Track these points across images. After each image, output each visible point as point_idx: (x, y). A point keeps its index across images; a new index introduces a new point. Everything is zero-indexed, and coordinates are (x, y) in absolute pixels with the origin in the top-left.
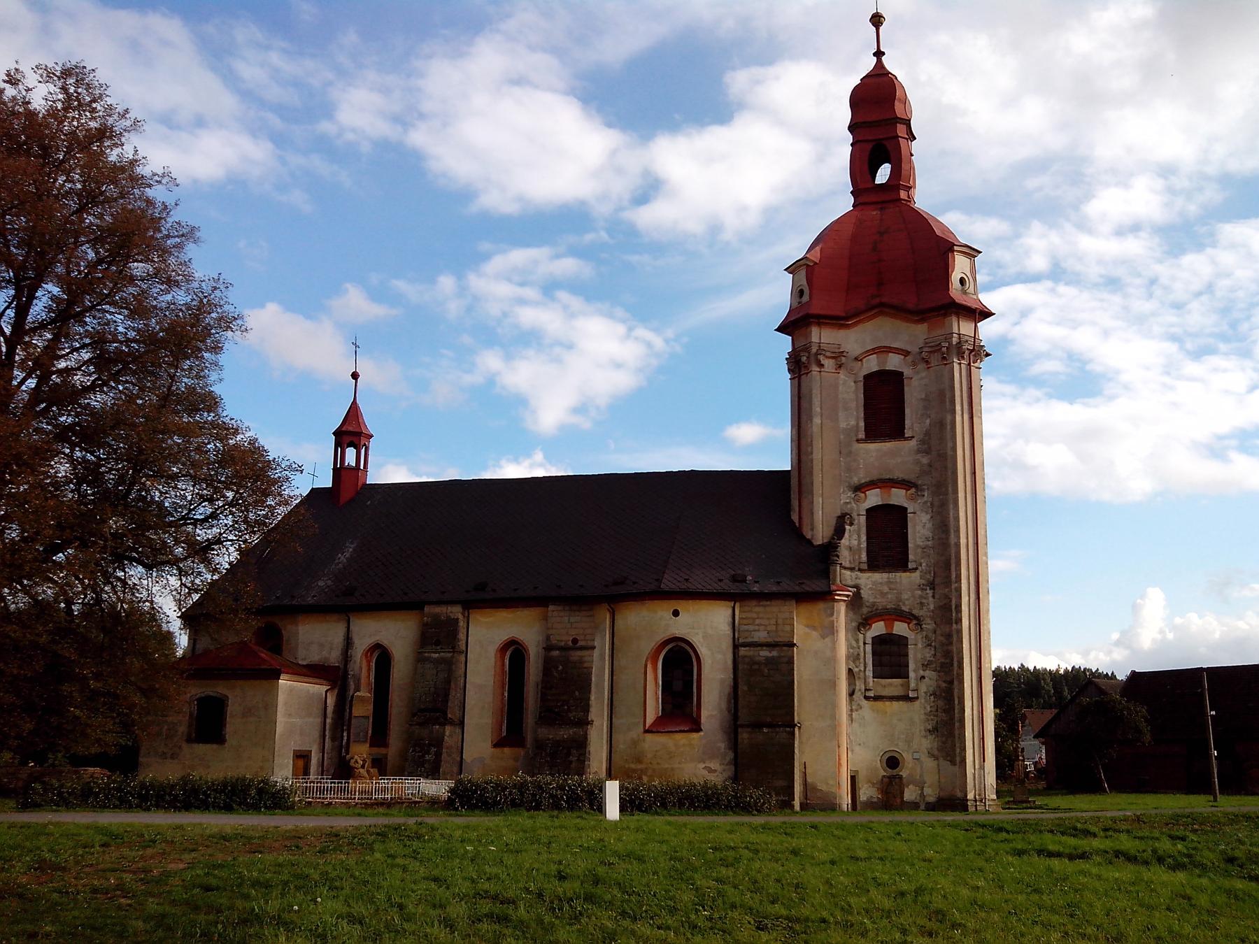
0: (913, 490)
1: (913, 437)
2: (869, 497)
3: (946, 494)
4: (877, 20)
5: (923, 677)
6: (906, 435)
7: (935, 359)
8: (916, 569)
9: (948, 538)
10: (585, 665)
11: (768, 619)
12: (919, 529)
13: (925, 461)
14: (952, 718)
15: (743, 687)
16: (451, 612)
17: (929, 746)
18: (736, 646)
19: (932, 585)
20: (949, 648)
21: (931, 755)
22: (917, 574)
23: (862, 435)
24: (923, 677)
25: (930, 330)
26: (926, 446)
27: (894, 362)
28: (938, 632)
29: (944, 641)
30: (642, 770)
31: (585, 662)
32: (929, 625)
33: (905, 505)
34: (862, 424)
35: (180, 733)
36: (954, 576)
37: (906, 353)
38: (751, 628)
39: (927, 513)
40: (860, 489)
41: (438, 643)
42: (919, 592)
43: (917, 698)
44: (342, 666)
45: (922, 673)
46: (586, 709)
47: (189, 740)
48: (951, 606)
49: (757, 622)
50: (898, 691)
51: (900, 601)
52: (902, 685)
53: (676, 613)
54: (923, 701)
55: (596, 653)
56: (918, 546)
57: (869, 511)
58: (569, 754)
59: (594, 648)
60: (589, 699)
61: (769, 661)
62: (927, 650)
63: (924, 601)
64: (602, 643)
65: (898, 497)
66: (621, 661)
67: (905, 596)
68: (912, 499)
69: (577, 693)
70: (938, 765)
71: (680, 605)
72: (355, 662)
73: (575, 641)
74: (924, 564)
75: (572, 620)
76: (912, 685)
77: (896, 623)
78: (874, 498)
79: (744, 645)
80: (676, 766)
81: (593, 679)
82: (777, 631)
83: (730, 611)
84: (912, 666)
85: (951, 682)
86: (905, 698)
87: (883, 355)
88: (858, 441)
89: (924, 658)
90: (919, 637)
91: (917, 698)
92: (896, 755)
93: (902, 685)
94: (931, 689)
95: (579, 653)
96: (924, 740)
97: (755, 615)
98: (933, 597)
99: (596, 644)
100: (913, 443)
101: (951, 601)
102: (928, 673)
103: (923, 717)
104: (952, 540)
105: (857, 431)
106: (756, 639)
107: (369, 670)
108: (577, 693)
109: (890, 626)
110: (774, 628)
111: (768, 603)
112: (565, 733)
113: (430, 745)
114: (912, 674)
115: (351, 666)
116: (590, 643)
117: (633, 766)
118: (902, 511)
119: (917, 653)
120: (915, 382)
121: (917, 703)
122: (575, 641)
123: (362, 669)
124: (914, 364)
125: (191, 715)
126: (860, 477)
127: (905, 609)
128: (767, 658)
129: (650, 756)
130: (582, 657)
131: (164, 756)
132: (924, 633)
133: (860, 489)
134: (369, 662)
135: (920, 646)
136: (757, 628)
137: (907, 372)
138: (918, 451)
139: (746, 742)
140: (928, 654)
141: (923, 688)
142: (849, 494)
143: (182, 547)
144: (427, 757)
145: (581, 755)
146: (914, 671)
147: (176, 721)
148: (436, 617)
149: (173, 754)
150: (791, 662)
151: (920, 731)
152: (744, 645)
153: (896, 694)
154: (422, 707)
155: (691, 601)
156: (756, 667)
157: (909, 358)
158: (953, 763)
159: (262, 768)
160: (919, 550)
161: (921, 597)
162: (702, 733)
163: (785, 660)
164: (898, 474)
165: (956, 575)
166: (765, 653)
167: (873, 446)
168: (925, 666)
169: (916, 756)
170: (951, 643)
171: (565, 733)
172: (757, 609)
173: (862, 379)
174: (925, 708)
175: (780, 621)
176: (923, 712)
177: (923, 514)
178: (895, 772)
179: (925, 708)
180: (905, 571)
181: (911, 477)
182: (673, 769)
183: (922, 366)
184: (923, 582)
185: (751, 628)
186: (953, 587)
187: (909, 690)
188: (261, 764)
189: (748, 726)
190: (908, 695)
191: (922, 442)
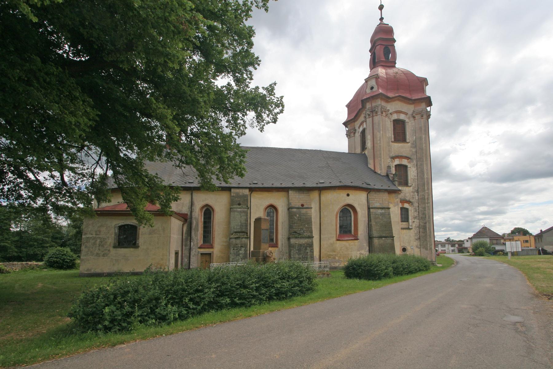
0: (410, 160)
1: (409, 142)
2: (395, 161)
3: (423, 161)
4: (381, 7)
5: (414, 222)
6: (407, 141)
7: (418, 117)
8: (411, 186)
9: (424, 176)
10: (309, 215)
11: (380, 199)
12: (412, 173)
13: (414, 150)
14: (426, 235)
15: (373, 223)
16: (244, 192)
17: (416, 244)
18: (369, 208)
19: (418, 192)
20: (425, 212)
21: (417, 247)
22: (411, 188)
23: (393, 140)
24: (414, 222)
25: (414, 107)
26: (414, 145)
27: (402, 117)
28: (420, 207)
29: (422, 210)
30: (335, 255)
31: (308, 213)
32: (416, 205)
33: (407, 165)
34: (393, 136)
35: (108, 243)
36: (426, 188)
37: (406, 114)
38: (374, 202)
39: (415, 167)
40: (393, 158)
41: (239, 204)
42: (412, 194)
43: (412, 229)
44: (189, 214)
45: (413, 220)
46: (311, 232)
47: (115, 247)
48: (425, 198)
49: (375, 200)
50: (406, 226)
51: (406, 196)
52: (406, 224)
53: (348, 195)
54: (414, 229)
55: (313, 210)
56: (412, 178)
57: (396, 166)
58: (306, 249)
59: (312, 208)
60: (312, 228)
61: (382, 214)
62: (415, 213)
63: (414, 196)
64: (315, 206)
65: (405, 162)
66: (324, 213)
67: (407, 195)
68: (409, 163)
69: (306, 226)
70: (420, 250)
71: (350, 192)
72: (196, 212)
73: (302, 205)
74: (414, 185)
75: (300, 197)
76: (410, 224)
77: (405, 204)
78: (397, 162)
79: (372, 208)
80: (349, 253)
81: (313, 220)
82: (383, 203)
83: (366, 196)
84: (410, 218)
85: (426, 223)
86: (408, 229)
87: (398, 114)
88: (392, 142)
89: (414, 215)
90: (412, 208)
91: (412, 229)
92: (404, 247)
93: (406, 224)
94: (417, 225)
95: (305, 210)
96: (415, 243)
97: (374, 197)
98: (418, 195)
99: (312, 206)
100: (409, 144)
101: (425, 196)
102: (415, 220)
103: (414, 235)
104: (426, 176)
105: (391, 139)
106: (376, 206)
107: (201, 216)
108: (306, 226)
109: (403, 205)
110: (382, 202)
111: (379, 193)
112: (303, 241)
113: (242, 247)
114: (410, 221)
115: (193, 214)
116: (309, 206)
117: (331, 253)
118: (406, 167)
119: (412, 213)
120: (410, 124)
121: (412, 230)
122: (302, 205)
123: (198, 216)
124: (409, 118)
125: (115, 233)
126: (393, 154)
127: (407, 199)
128: (381, 213)
129: (339, 249)
130: (306, 211)
131: (98, 255)
132: (414, 207)
133: (393, 158)
134: (201, 212)
135: (412, 211)
136: (376, 202)
137: (407, 120)
138: (411, 147)
139: (377, 243)
140: (416, 214)
141: (414, 225)
142: (390, 159)
143: (222, 28)
144: (241, 252)
145: (311, 249)
146: (411, 219)
147: (105, 237)
148: (237, 194)
149: (104, 254)
150: (389, 214)
151: (413, 239)
152: (372, 208)
153: (404, 227)
154: (235, 231)
155: (354, 191)
156: (377, 216)
157: (408, 116)
158: (426, 249)
159: (162, 259)
160: (412, 180)
161: (413, 195)
162: (359, 240)
163: (387, 214)
164: (405, 155)
165: (427, 188)
166: (380, 211)
167: (396, 144)
168: (415, 218)
169: (412, 247)
170: (425, 210)
171: (303, 241)
172: (374, 195)
173: (392, 121)
174: (415, 232)
175: (384, 200)
176: (414, 233)
177: (413, 168)
178: (405, 253)
179: (415, 232)
180: (407, 187)
181: (408, 156)
182: (348, 254)
183: (412, 119)
184: (413, 190)
185: (374, 202)
186: (426, 192)
187: (409, 226)
188: (161, 257)
189: (377, 237)
190: (409, 227)
191: (413, 144)
